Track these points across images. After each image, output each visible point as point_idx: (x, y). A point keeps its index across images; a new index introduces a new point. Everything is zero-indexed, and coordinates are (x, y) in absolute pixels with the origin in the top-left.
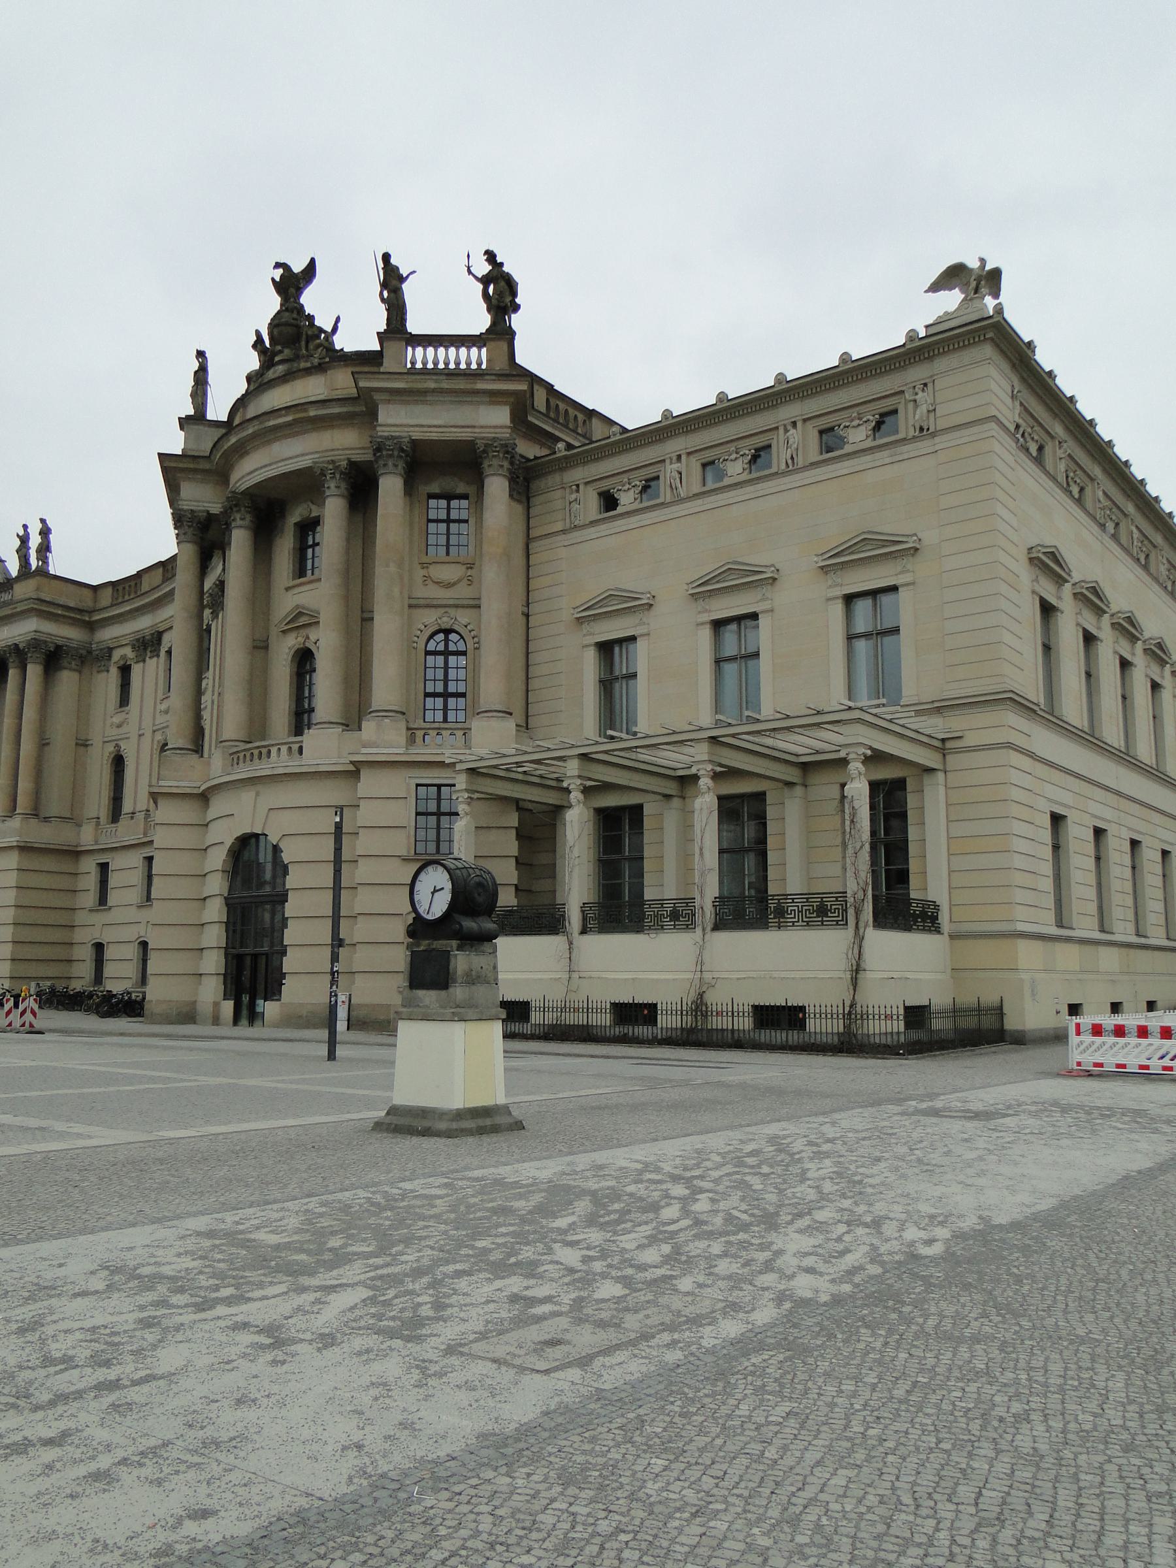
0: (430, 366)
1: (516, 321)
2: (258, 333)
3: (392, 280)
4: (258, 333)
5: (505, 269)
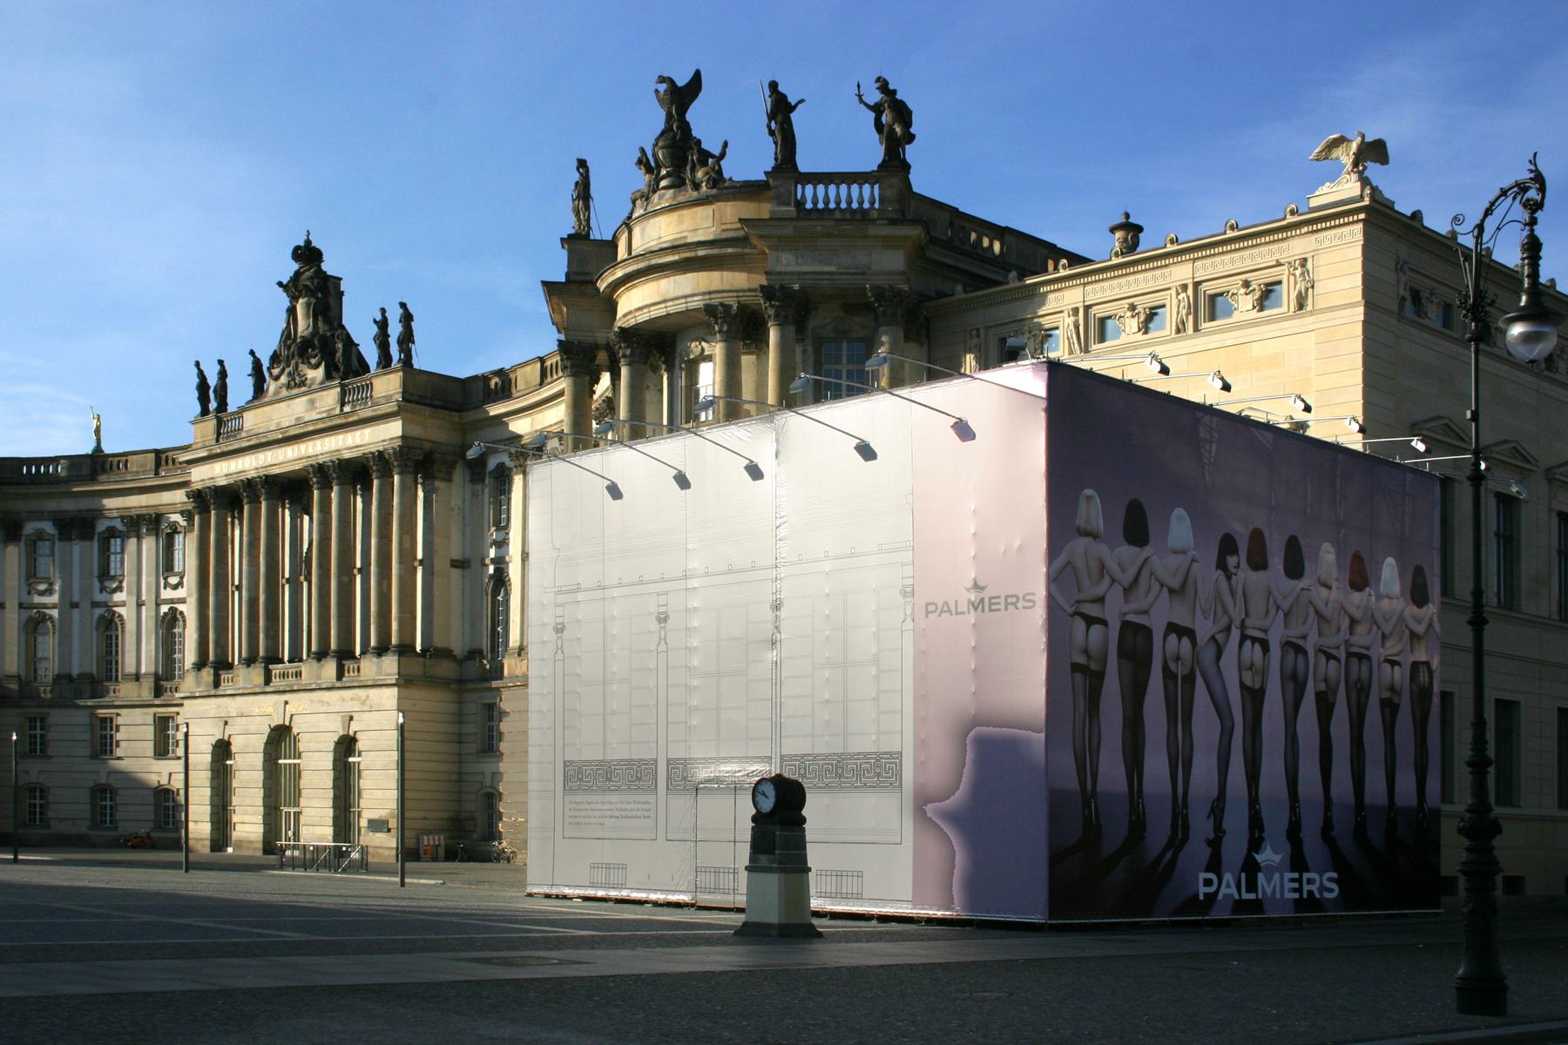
0: (821, 206)
1: (911, 153)
2: (643, 150)
3: (781, 109)
4: (643, 150)
5: (898, 97)
